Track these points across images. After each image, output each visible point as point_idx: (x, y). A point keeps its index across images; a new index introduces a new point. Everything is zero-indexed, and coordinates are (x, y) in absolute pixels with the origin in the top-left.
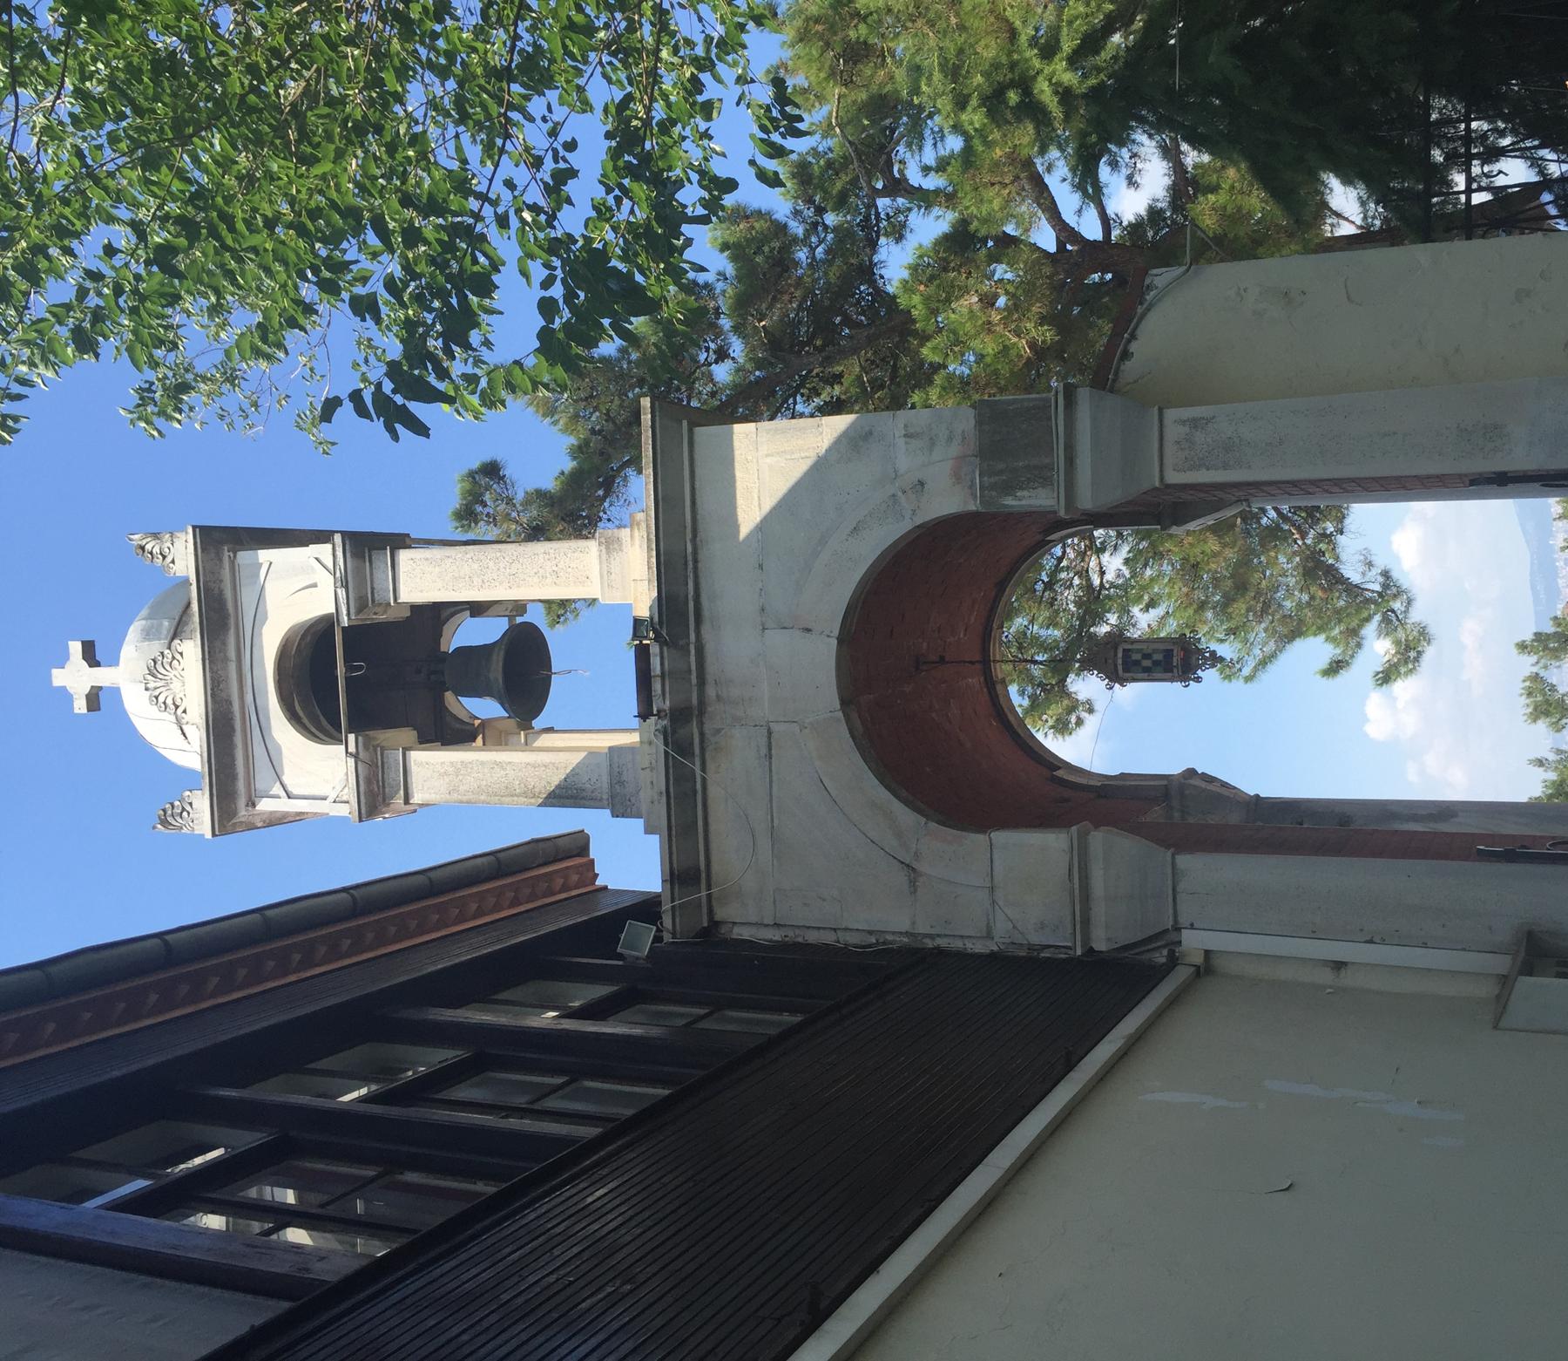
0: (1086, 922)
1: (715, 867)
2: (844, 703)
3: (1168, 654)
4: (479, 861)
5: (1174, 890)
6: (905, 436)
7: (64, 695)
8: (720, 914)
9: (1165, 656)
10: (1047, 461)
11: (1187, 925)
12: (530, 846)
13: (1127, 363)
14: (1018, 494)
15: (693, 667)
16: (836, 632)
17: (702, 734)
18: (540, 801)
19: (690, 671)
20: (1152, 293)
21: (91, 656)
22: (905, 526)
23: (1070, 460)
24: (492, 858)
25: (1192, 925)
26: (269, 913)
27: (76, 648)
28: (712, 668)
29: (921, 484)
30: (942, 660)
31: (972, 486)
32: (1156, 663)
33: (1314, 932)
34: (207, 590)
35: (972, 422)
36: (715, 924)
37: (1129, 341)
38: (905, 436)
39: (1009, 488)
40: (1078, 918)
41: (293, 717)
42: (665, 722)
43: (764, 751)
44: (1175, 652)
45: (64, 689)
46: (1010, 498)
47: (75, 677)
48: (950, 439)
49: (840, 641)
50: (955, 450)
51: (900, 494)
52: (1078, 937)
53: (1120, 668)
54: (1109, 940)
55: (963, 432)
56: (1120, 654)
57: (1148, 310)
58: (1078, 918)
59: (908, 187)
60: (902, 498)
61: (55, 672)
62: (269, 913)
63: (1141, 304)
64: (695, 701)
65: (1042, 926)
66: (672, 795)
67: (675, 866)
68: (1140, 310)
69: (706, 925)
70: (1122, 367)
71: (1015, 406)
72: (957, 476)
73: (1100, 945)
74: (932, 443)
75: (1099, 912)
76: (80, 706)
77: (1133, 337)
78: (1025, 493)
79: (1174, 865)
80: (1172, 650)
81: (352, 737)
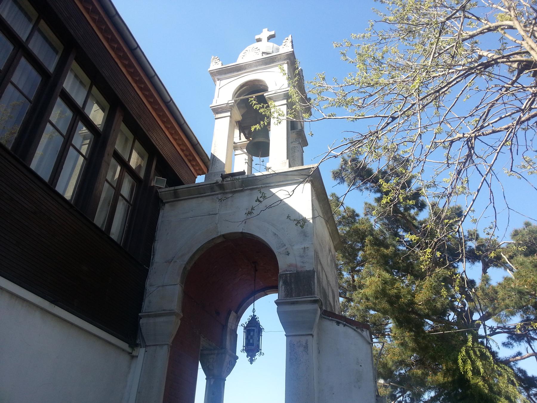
0: (149, 316)
1: (182, 202)
2: (224, 236)
3: (252, 344)
4: (194, 138)
5: (157, 345)
6: (305, 248)
7: (260, 32)
8: (167, 205)
9: (251, 343)
10: (293, 295)
11: (147, 350)
12: (205, 154)
13: (336, 324)
14: (283, 286)
15: (237, 189)
16: (244, 231)
17: (217, 194)
18: (213, 153)
19: (236, 189)
20: (360, 331)
21: (270, 38)
22: (276, 251)
23: (293, 303)
24: (197, 143)
25: (146, 351)
26: (156, 77)
27: (272, 33)
28: (236, 195)
29: (288, 254)
30: (256, 270)
31: (287, 271)
32: (249, 340)
33: (139, 392)
34: (276, 58)
35: (308, 269)
36: (164, 204)
37: (343, 324)
38: (305, 248)
39: (285, 283)
40: (149, 313)
41: (242, 86)
42: (220, 183)
43: (211, 213)
44: (252, 347)
45: (262, 32)
46: (282, 284)
47: (265, 34)
48: (303, 262)
49: (242, 233)
50: (299, 264)
51: (286, 247)
52: (145, 314)
53: (248, 328)
54: (143, 324)
55: (305, 267)
56: (253, 328)
57: (355, 330)
58: (149, 313)
59: (486, 269)
60: (284, 248)
61: (267, 29)
62: (156, 77)
63: (356, 328)
64: (226, 191)
65: (150, 302)
66: (199, 187)
67: (179, 190)
68: (354, 327)
69: (164, 201)
70: (334, 322)
71: (312, 283)
72: (291, 265)
73: (141, 321)
74: (301, 257)
75: (152, 320)
76: (257, 37)
77: (345, 325)
78: (283, 289)
79: (165, 344)
80: (253, 346)
81: (233, 101)
